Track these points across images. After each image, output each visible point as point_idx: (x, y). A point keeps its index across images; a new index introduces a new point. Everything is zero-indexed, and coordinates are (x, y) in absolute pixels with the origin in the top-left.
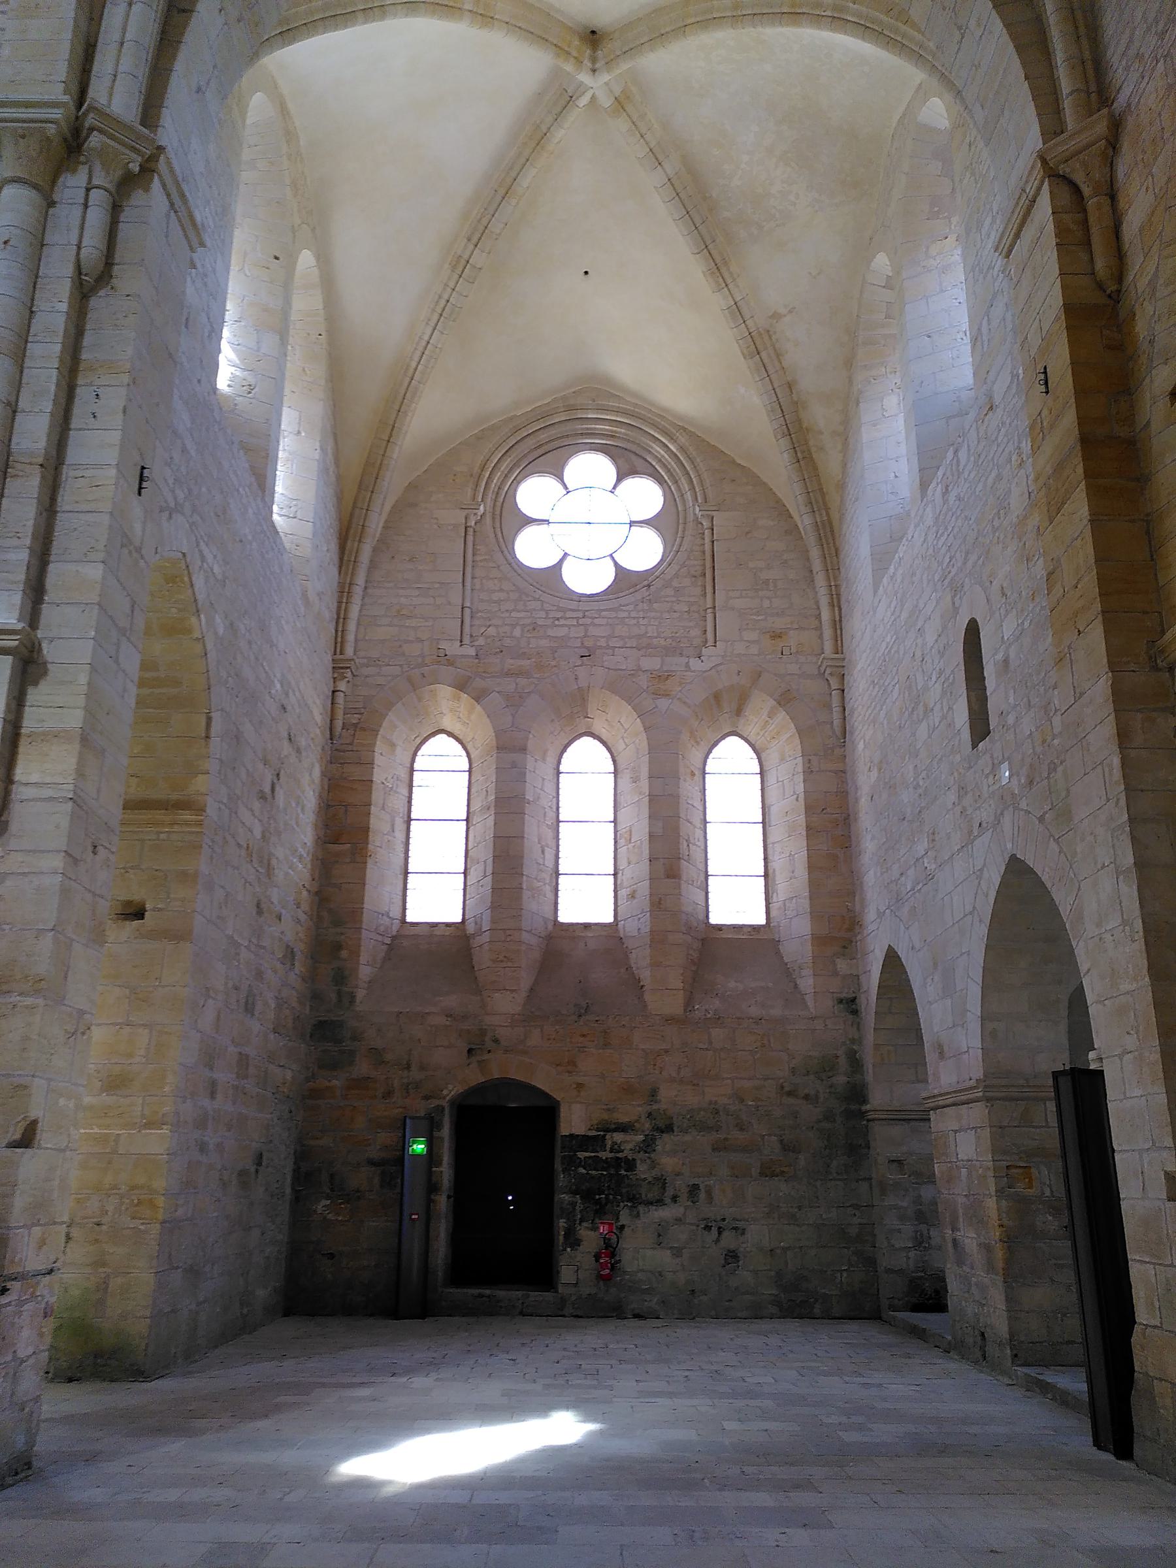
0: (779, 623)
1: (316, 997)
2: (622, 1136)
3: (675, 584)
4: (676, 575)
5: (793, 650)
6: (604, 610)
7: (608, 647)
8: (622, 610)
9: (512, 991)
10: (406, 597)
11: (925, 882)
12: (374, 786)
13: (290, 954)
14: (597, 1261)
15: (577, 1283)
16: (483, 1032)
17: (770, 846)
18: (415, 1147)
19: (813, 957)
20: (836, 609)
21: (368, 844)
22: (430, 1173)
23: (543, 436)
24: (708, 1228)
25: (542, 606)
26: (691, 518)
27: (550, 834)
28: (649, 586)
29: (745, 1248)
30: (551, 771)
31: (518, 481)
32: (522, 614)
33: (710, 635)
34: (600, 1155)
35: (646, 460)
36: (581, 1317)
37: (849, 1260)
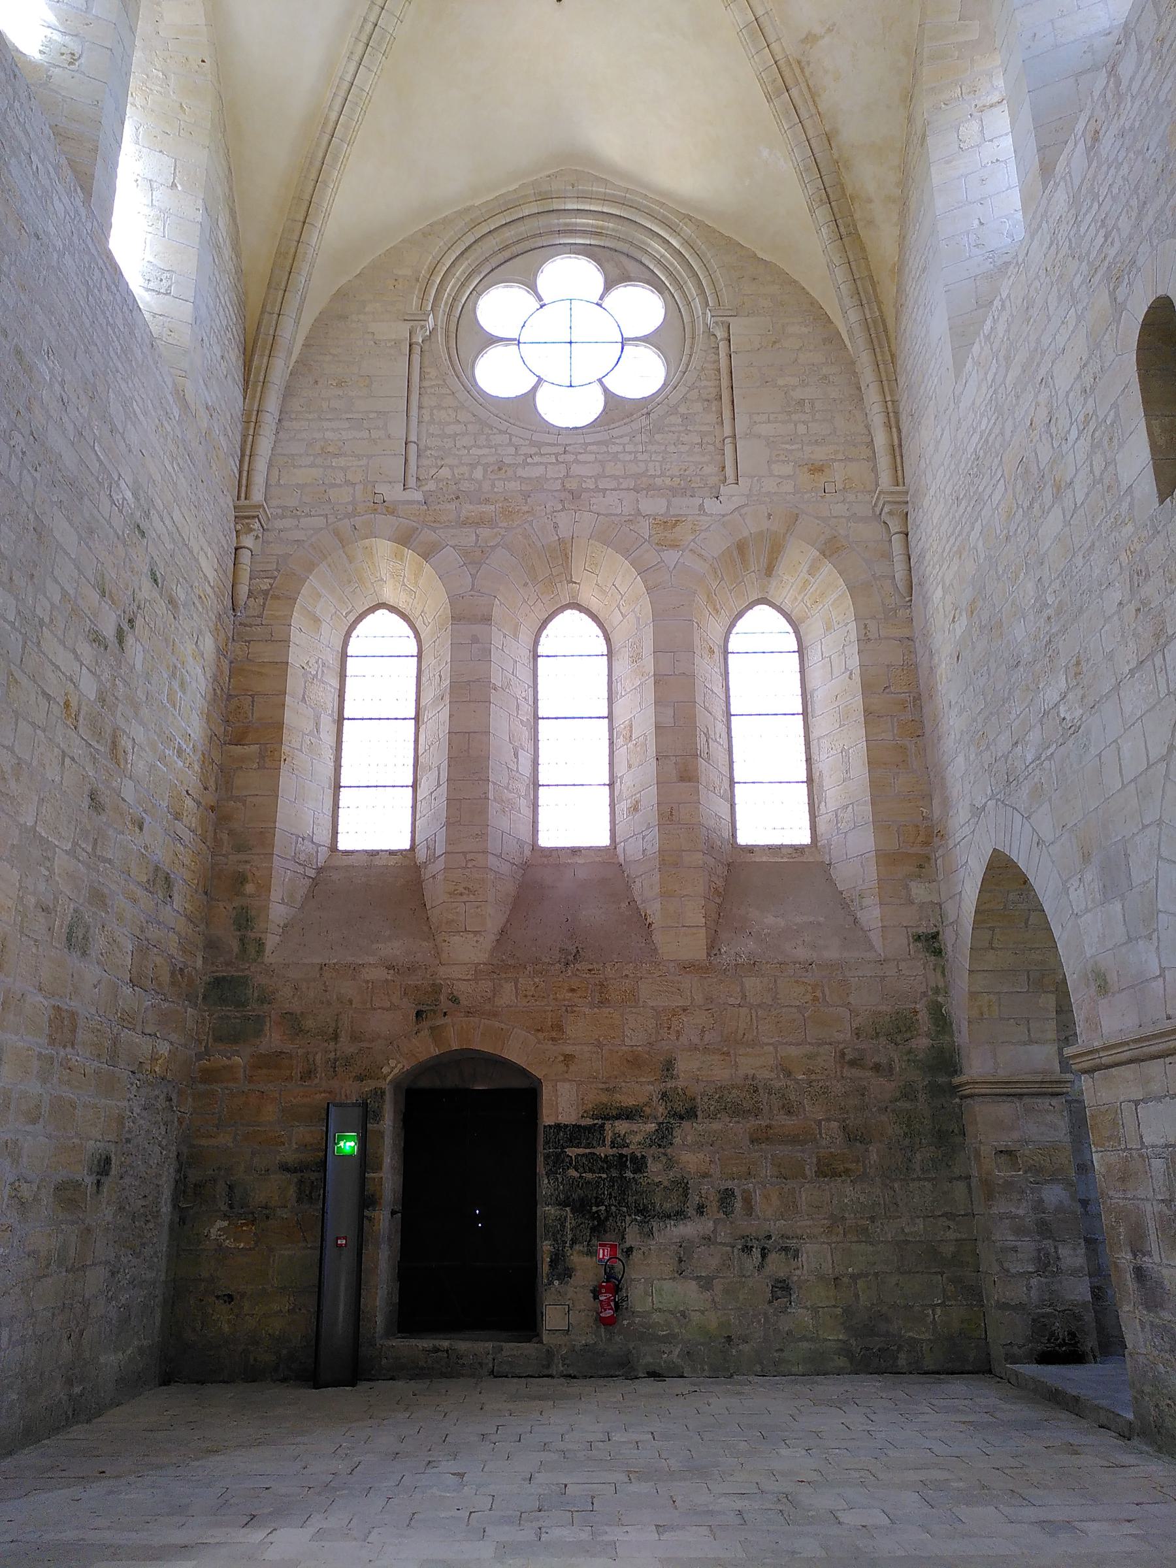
0: (819, 454)
1: (212, 946)
2: (627, 1125)
3: (682, 409)
4: (684, 399)
5: (840, 486)
6: (590, 444)
7: (597, 489)
8: (614, 444)
9: (476, 933)
10: (333, 430)
11: (1061, 741)
13: (161, 881)
14: (596, 1298)
15: (568, 1330)
16: (436, 989)
17: (814, 744)
18: (342, 1144)
19: (879, 880)
20: (894, 430)
22: (363, 1181)
23: (509, 234)
24: (747, 1249)
25: (510, 440)
26: (701, 328)
27: (526, 734)
29: (799, 1277)
30: (524, 654)
31: (477, 292)
32: (486, 451)
33: (729, 471)
34: (597, 1151)
36: (575, 1377)
37: (944, 1290)
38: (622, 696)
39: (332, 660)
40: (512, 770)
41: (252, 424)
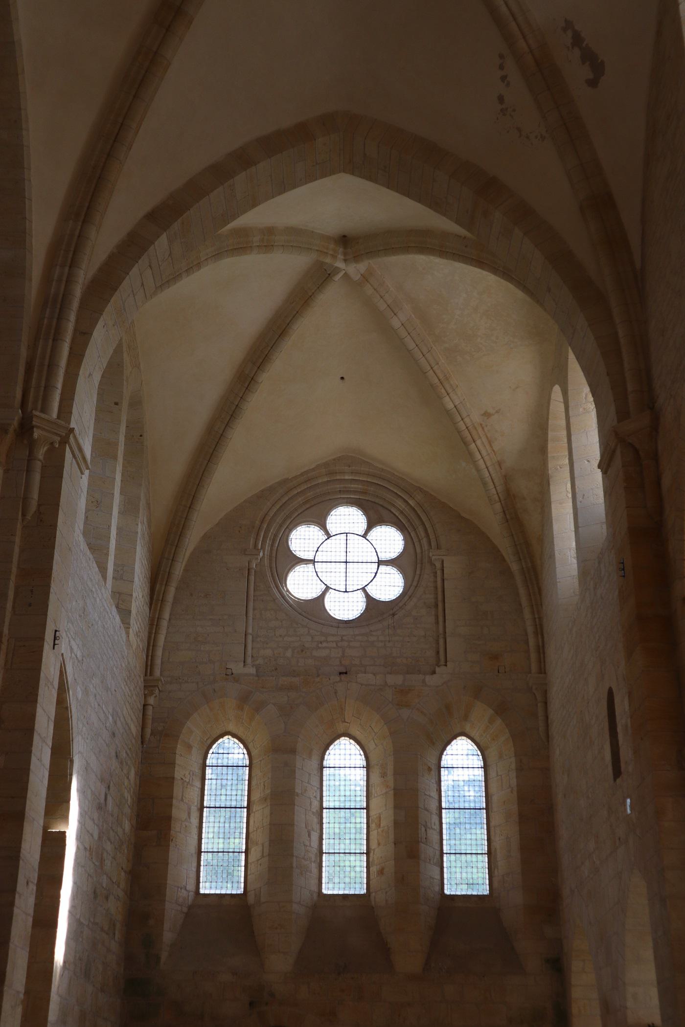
12: (176, 782)
17: (492, 829)
20: (540, 636)
21: (170, 830)
25: (309, 632)
27: (315, 820)
28: (394, 615)
31: (290, 529)
35: (390, 511)
38: (375, 797)
39: (197, 770)
40: (307, 846)
41: (155, 626)
